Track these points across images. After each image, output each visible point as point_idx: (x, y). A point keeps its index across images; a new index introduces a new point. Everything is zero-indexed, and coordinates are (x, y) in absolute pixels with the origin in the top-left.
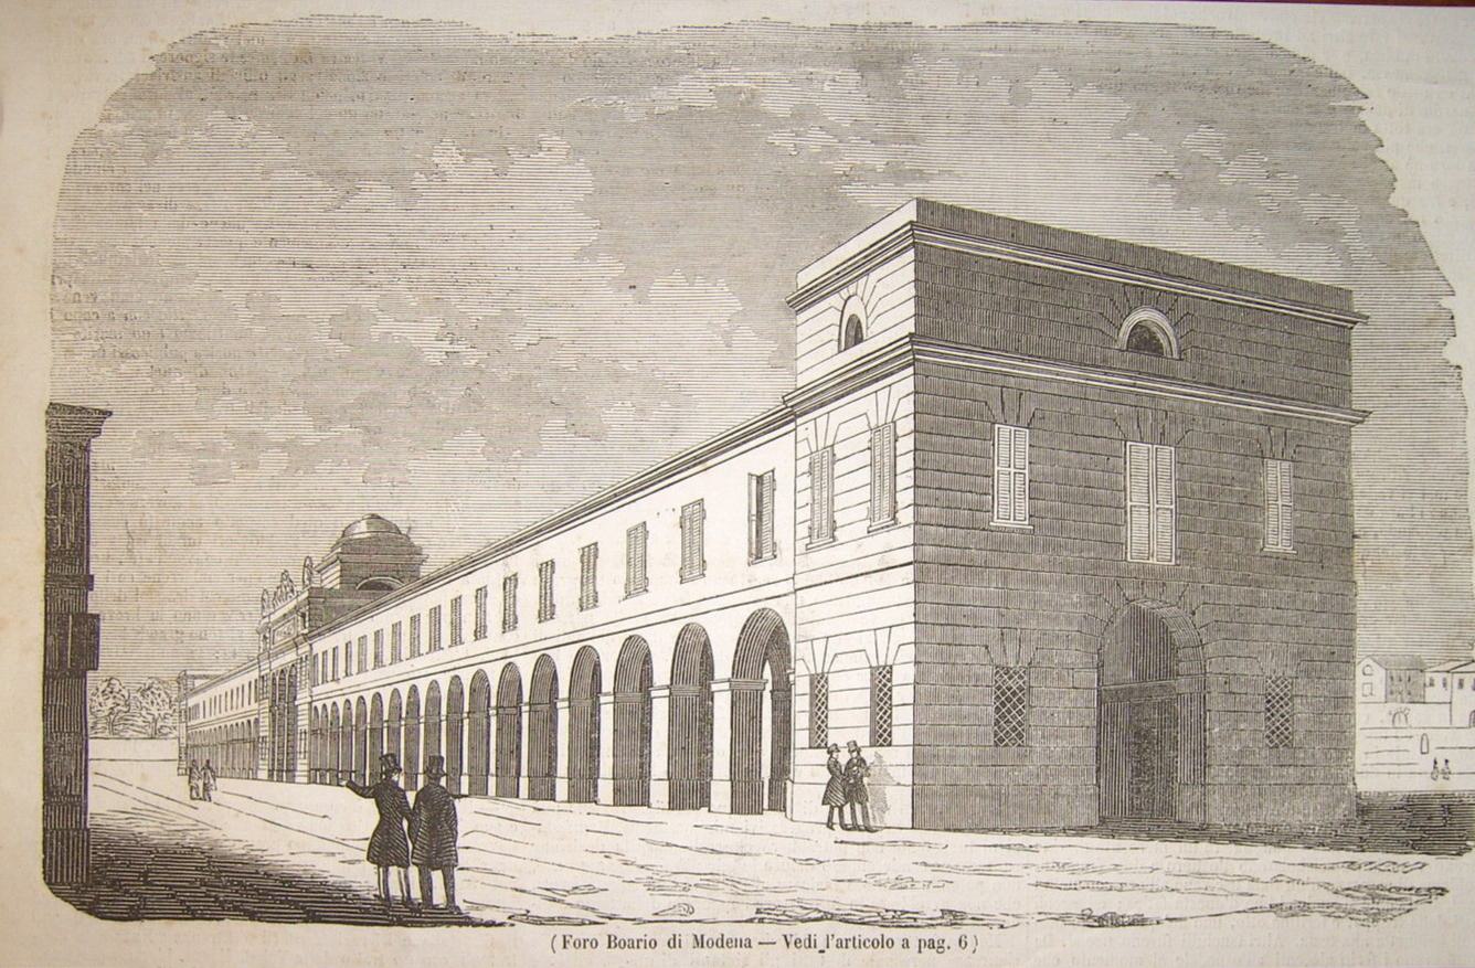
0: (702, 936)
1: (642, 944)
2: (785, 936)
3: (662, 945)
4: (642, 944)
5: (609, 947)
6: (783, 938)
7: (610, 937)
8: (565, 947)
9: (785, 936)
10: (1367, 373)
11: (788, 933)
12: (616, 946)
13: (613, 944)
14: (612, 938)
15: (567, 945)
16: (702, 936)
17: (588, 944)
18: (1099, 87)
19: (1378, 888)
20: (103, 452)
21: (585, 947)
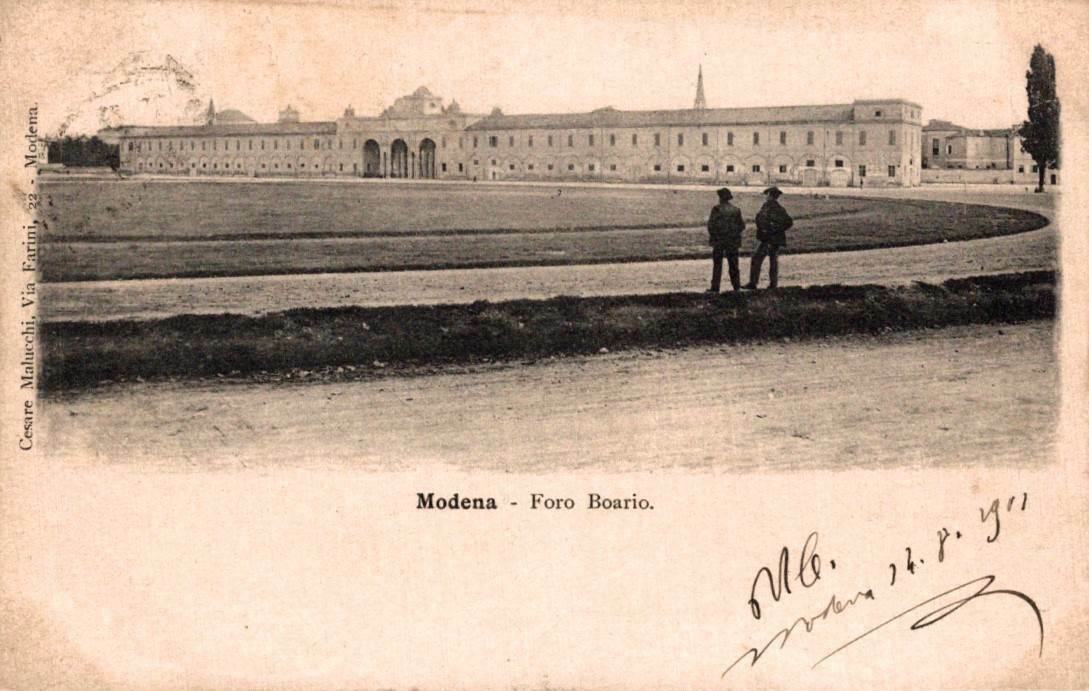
0: (27, 157)
1: (631, 504)
2: (24, 305)
3: (1055, 172)
4: (631, 504)
5: (591, 506)
6: (26, 307)
7: (591, 496)
8: (534, 507)
9: (24, 305)
10: (1057, 203)
11: (20, 302)
12: (599, 505)
13: (595, 504)
14: (595, 498)
15: (537, 504)
16: (23, 378)
17: (562, 504)
18: (799, 315)
19: (283, 460)
20: (654, 141)
21: (558, 507)
